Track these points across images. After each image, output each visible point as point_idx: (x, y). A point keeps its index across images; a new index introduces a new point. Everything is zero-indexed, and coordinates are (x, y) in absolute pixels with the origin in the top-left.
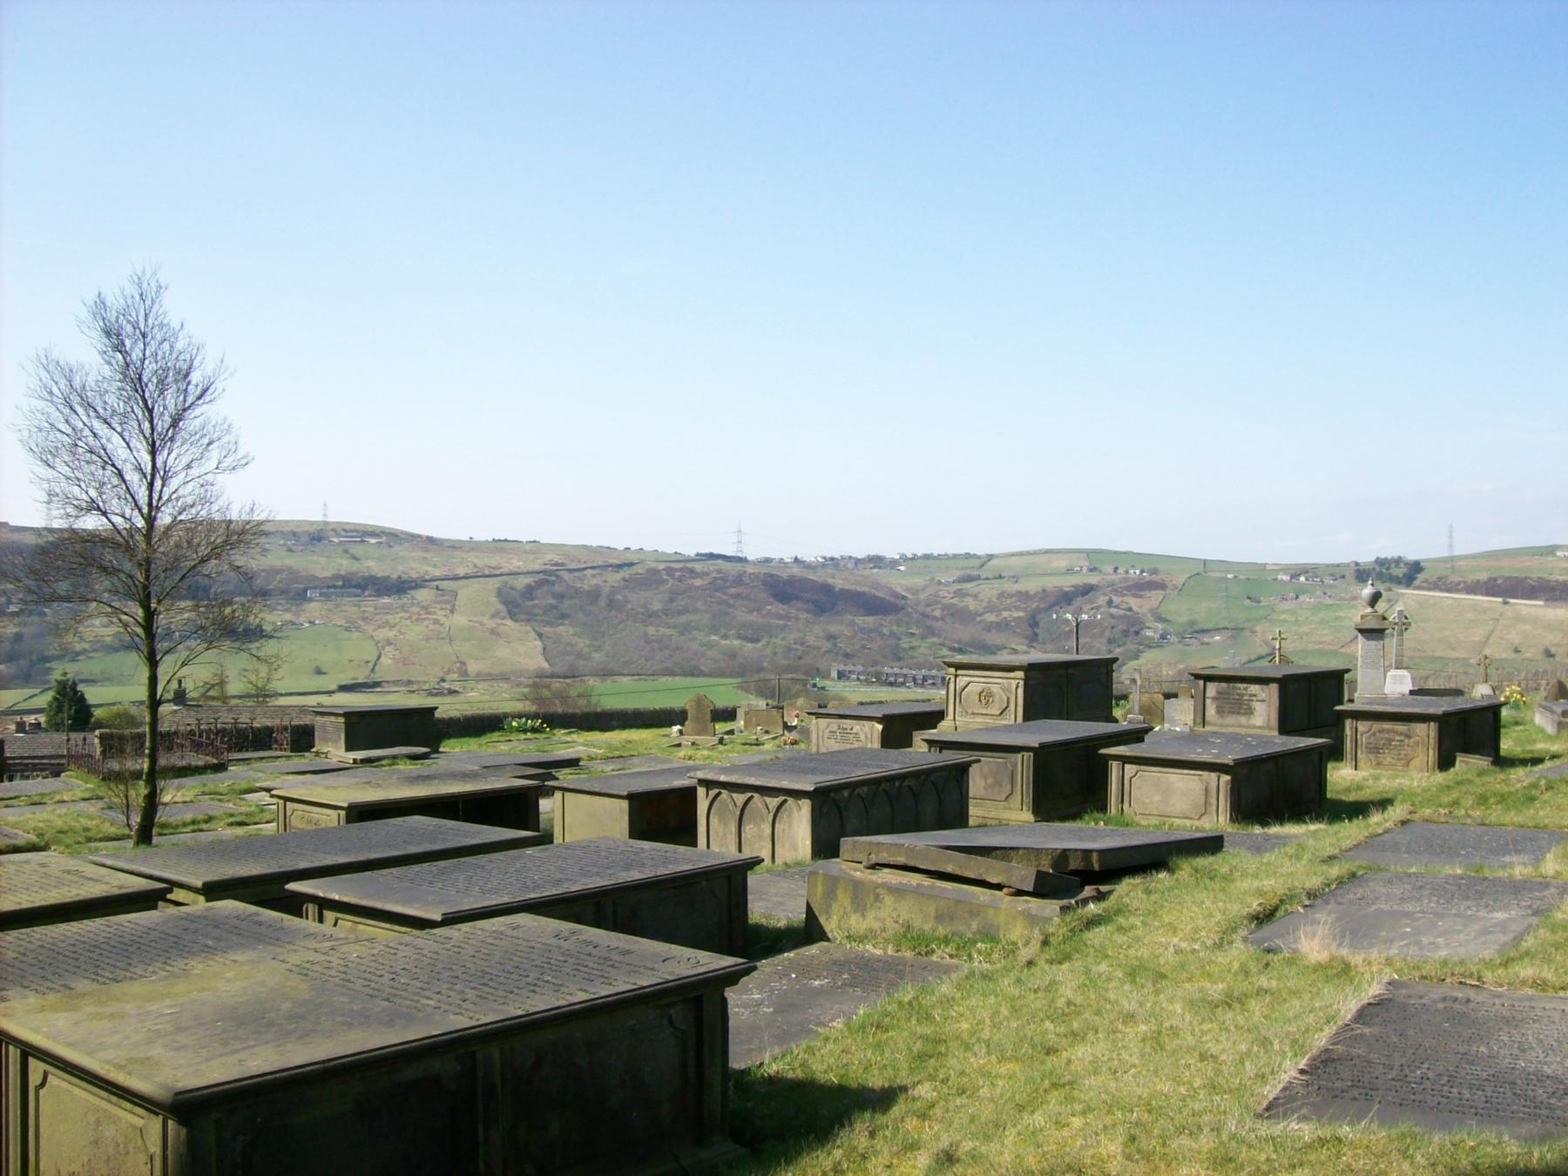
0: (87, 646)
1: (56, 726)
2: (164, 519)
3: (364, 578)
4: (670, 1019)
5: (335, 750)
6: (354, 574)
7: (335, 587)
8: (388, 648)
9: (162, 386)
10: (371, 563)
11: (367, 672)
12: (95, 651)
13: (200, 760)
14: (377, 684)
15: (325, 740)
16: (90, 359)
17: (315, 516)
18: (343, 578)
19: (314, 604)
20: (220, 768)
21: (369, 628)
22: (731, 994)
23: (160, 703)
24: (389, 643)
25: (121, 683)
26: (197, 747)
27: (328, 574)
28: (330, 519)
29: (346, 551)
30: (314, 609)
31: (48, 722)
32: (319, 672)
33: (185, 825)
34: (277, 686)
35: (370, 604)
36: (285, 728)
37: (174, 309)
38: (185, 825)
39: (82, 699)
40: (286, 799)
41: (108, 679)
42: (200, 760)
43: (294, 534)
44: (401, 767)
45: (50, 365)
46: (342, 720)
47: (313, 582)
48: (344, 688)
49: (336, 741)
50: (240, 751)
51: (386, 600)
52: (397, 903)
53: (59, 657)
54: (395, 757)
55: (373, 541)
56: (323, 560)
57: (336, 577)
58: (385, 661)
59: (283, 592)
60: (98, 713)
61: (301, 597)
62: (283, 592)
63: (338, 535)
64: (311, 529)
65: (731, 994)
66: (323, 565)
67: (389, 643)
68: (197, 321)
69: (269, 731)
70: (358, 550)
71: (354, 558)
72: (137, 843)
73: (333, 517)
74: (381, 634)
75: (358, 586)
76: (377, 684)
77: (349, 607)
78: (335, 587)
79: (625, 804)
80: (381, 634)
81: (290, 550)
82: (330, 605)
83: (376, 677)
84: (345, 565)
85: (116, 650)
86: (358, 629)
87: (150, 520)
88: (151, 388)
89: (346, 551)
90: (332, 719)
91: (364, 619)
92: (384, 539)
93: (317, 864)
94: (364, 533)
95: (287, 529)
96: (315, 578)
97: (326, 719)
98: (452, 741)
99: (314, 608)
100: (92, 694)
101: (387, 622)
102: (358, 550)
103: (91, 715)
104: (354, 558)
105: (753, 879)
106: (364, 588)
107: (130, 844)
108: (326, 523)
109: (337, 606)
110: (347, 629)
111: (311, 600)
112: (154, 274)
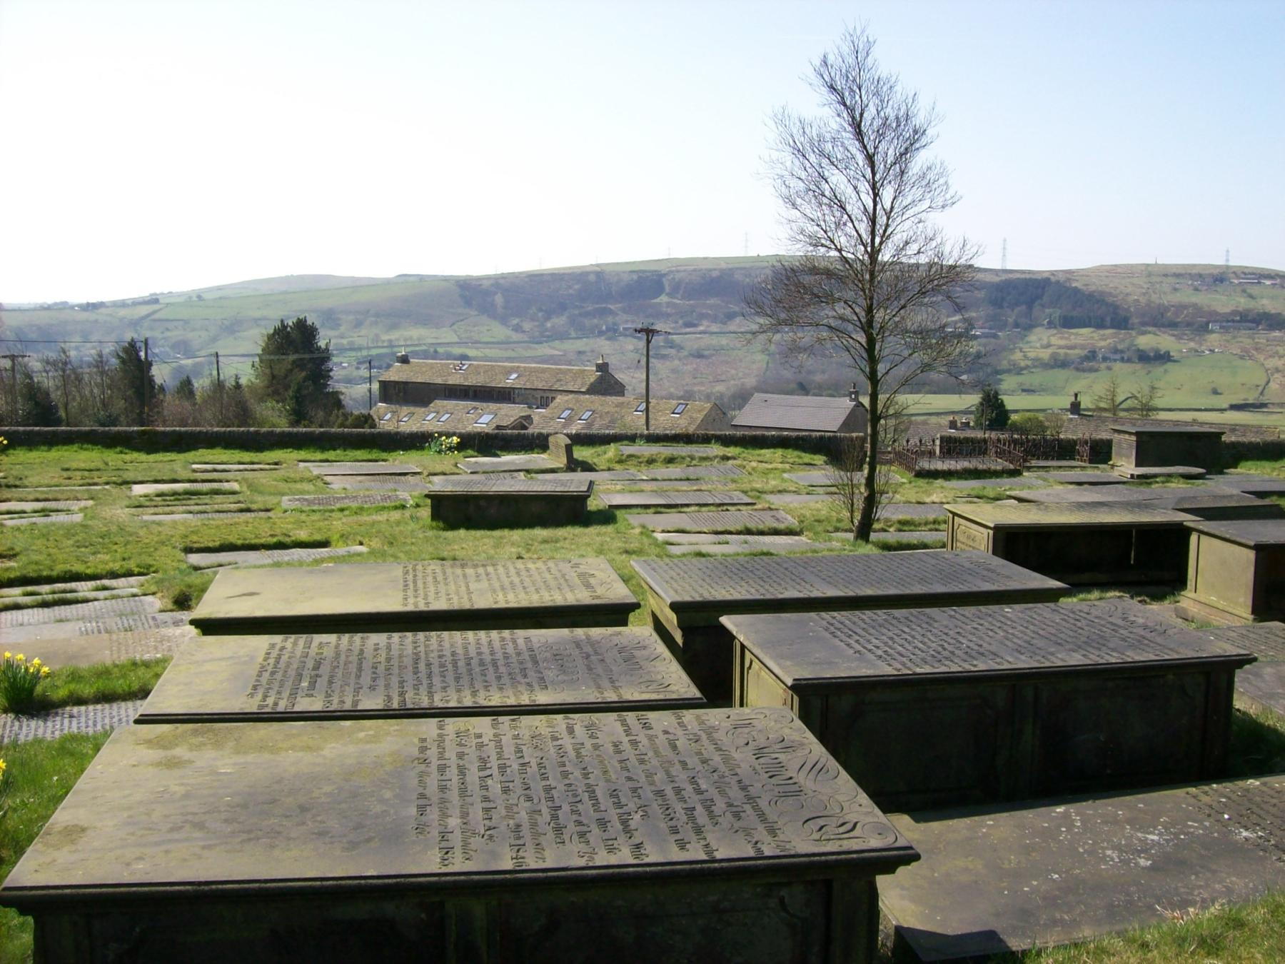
0: (1029, 363)
1: (979, 425)
2: (885, 256)
3: (1259, 314)
4: (782, 900)
5: (1125, 466)
6: (1249, 311)
7: (1233, 321)
8: (1276, 375)
9: (880, 135)
10: (1265, 301)
11: (1256, 394)
12: (1035, 367)
13: (1000, 464)
14: (1264, 405)
15: (1120, 455)
16: (824, 115)
17: (1220, 261)
18: (1241, 314)
19: (1214, 336)
20: (1015, 473)
21: (1261, 357)
22: (882, 881)
23: (879, 418)
24: (1277, 370)
25: (1055, 394)
26: (1000, 454)
27: (1227, 310)
28: (1231, 263)
29: (1244, 291)
30: (1214, 339)
31: (976, 422)
32: (1215, 392)
33: (926, 524)
34: (1158, 402)
35: (1262, 337)
36: (1086, 442)
37: (884, 63)
38: (926, 524)
39: (1002, 405)
40: (954, 514)
41: (1043, 390)
42: (1000, 464)
43: (1200, 275)
44: (1173, 485)
45: (781, 120)
46: (1134, 438)
47: (1214, 317)
48: (1235, 407)
49: (1128, 457)
50: (1047, 459)
51: (1277, 334)
52: (771, 658)
53: (1008, 371)
54: (1170, 475)
55: (1268, 282)
56: (1224, 298)
57: (1234, 313)
58: (1273, 386)
59: (1189, 325)
60: (1014, 417)
61: (1203, 329)
62: (1189, 325)
63: (1238, 277)
64: (1216, 272)
65: (882, 881)
66: (1223, 302)
67: (1277, 370)
68: (911, 73)
69: (1072, 444)
70: (1254, 290)
71: (1251, 296)
72: (856, 538)
73: (1235, 261)
74: (1272, 363)
75: (1253, 321)
76: (1264, 405)
77: (1244, 339)
78: (1233, 321)
79: (1251, 555)
80: (1272, 363)
81: (1196, 289)
82: (1228, 337)
83: (1264, 399)
84: (1242, 303)
85: (1052, 367)
86: (1251, 357)
87: (874, 254)
88: (875, 135)
89: (1244, 291)
90: (1127, 436)
91: (1256, 349)
92: (1278, 281)
93: (816, 594)
94: (1261, 276)
95: (1194, 271)
96: (1217, 313)
97: (1122, 436)
98: (1249, 463)
99: (1214, 339)
100: (1010, 402)
101: (1277, 353)
102: (1254, 290)
103: (1008, 418)
104: (1251, 296)
105: (1239, 675)
106: (1258, 323)
107: (851, 536)
108: (1228, 267)
109: (1234, 337)
110: (1242, 358)
111: (1212, 332)
112: (863, 32)
